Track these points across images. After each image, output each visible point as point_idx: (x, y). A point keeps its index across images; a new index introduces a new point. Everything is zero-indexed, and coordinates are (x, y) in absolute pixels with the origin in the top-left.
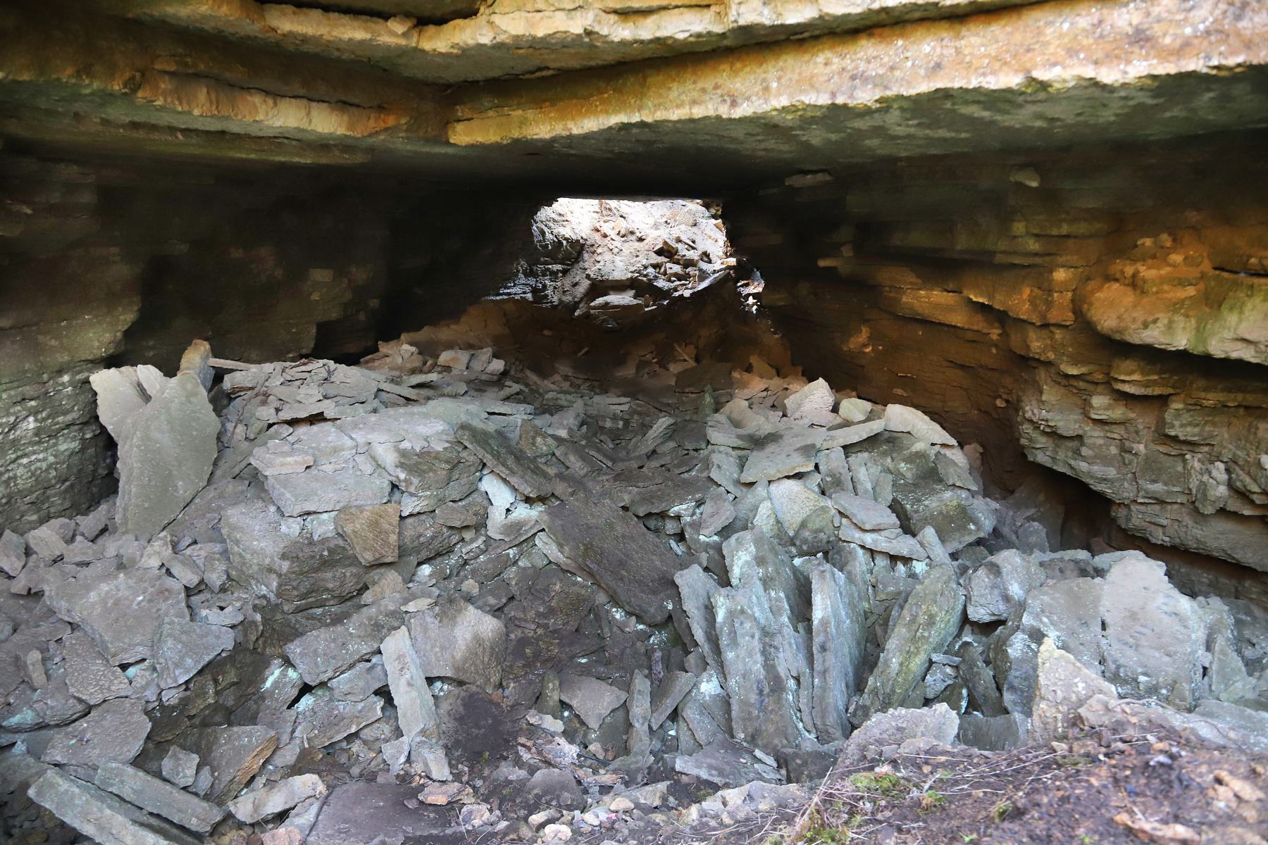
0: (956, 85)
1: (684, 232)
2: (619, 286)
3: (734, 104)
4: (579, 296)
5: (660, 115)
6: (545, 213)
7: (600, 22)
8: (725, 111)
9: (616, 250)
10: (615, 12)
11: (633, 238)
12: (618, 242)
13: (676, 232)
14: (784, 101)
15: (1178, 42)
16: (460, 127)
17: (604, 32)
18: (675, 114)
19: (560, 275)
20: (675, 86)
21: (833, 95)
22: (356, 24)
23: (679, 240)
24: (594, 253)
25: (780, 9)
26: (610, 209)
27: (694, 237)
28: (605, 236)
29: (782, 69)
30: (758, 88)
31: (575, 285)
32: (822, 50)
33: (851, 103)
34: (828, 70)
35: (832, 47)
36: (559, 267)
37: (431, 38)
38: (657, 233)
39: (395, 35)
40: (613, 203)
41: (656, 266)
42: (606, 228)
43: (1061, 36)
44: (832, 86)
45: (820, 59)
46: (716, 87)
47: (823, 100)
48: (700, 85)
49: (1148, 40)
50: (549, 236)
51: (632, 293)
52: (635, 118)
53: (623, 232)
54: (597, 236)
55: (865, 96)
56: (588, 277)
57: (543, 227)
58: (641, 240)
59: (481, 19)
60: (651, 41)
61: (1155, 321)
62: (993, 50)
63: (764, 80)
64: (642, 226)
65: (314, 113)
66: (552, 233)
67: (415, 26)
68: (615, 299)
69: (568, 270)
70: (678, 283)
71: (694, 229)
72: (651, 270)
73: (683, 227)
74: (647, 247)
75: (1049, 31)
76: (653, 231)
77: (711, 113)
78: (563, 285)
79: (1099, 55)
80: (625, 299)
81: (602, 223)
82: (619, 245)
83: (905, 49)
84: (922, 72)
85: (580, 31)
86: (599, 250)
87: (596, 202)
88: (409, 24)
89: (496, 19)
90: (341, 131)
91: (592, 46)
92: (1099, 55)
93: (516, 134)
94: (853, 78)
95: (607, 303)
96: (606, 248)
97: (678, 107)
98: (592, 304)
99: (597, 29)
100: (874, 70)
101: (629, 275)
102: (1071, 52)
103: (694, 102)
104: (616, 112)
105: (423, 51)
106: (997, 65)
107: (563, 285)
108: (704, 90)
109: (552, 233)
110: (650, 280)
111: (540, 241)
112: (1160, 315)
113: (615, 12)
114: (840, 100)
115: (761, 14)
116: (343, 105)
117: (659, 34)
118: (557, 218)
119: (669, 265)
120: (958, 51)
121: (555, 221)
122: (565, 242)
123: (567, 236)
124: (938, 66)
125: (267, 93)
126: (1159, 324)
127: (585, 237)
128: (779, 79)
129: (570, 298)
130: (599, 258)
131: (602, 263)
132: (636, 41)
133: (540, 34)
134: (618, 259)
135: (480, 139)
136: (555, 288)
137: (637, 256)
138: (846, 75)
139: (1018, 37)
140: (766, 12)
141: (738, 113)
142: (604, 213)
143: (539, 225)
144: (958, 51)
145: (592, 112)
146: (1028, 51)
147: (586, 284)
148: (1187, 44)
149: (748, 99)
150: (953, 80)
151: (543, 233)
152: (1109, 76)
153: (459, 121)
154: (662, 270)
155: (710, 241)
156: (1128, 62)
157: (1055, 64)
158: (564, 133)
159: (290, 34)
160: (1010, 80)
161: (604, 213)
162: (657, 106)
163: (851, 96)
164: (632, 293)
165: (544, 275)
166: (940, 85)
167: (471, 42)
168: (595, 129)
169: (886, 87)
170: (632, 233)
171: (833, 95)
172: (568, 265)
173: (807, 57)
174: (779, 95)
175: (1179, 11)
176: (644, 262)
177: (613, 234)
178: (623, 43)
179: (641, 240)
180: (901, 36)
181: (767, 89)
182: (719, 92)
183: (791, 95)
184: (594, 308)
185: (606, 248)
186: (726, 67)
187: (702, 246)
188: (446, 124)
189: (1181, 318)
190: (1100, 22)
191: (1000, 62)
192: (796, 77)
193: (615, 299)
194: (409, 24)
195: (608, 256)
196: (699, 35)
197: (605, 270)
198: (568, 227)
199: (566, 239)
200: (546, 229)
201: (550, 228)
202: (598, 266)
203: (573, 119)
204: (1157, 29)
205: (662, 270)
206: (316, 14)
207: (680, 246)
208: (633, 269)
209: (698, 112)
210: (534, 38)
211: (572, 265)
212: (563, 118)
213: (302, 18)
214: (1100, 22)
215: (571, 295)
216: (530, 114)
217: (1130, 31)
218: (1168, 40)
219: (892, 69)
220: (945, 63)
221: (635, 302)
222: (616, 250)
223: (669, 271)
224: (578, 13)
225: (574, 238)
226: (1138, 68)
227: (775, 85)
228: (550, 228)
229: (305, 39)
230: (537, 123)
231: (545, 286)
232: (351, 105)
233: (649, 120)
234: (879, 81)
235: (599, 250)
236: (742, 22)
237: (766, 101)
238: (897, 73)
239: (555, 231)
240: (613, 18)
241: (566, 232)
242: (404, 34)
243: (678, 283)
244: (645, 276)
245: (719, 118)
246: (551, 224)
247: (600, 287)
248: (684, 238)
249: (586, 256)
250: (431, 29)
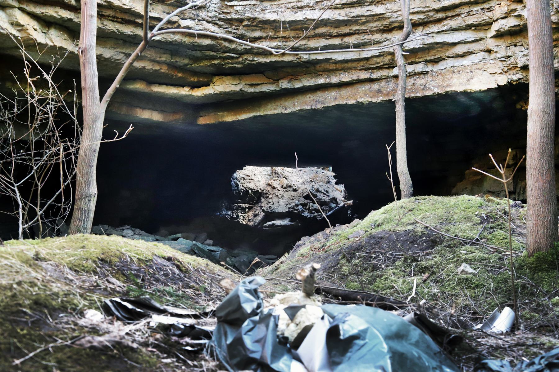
0: (341, 103)
1: (321, 186)
2: (281, 216)
3: (286, 109)
4: (258, 221)
5: (265, 113)
6: (239, 174)
7: (244, 88)
8: (283, 111)
9: (280, 196)
10: (249, 85)
11: (291, 189)
12: (282, 191)
13: (316, 186)
14: (299, 108)
15: (387, 92)
16: (201, 119)
17: (246, 90)
18: (269, 113)
19: (247, 210)
20: (269, 104)
21: (312, 106)
22: (175, 88)
23: (318, 190)
24: (267, 197)
25: (293, 84)
26: (278, 174)
27: (328, 189)
28: (274, 188)
29: (298, 99)
30: (292, 105)
31: (255, 216)
32: (308, 94)
33: (316, 108)
34: (310, 99)
35: (311, 93)
36: (247, 205)
37: (196, 92)
38: (304, 187)
39: (186, 91)
40: (279, 169)
41: (304, 205)
42: (275, 184)
43: (363, 91)
44: (311, 104)
45: (308, 97)
46: (281, 105)
47: (309, 108)
48: (276, 104)
49: (381, 92)
50: (241, 187)
51: (289, 219)
52: (258, 114)
53: (285, 186)
54: (269, 188)
55: (319, 106)
56: (263, 211)
57: (238, 182)
58: (295, 190)
59: (211, 87)
60: (259, 92)
61: (466, 188)
62: (348, 94)
63: (294, 102)
64: (296, 183)
65: (153, 114)
66: (243, 186)
67: (191, 89)
68: (278, 222)
69: (252, 207)
70: (316, 214)
71: (328, 185)
72: (300, 207)
73: (321, 184)
74: (299, 195)
75: (360, 89)
76: (303, 186)
77: (280, 112)
78: (249, 216)
79: (371, 95)
80: (285, 222)
81: (272, 181)
82: (282, 193)
83: (328, 94)
84: (332, 100)
85: (238, 90)
86: (270, 196)
87: (269, 169)
88: (189, 88)
89: (214, 87)
90: (161, 120)
91: (242, 94)
92: (371, 95)
93: (220, 120)
94: (316, 101)
95: (273, 224)
96: (274, 195)
97: (270, 110)
98: (265, 225)
99: (243, 89)
100: (321, 99)
101: (287, 210)
102: (365, 95)
103: (275, 109)
104: (252, 112)
105: (193, 95)
106: (350, 98)
107: (249, 216)
108: (277, 105)
109: (243, 186)
110: (299, 212)
111: (235, 190)
112: (468, 186)
113: (249, 85)
114: (313, 108)
115: (287, 85)
116: (162, 111)
117: (261, 90)
118: (246, 177)
119: (311, 204)
120: (340, 95)
121: (244, 179)
122: (250, 191)
123: (252, 188)
124: (336, 98)
125: (141, 108)
126: (467, 189)
127: (262, 189)
128: (298, 102)
129: (253, 223)
130: (270, 201)
131: (272, 203)
132: (255, 92)
133: (227, 91)
134: (281, 201)
135: (208, 122)
136: (244, 217)
137: (293, 199)
138: (314, 101)
139: (353, 91)
140: (289, 85)
141: (287, 112)
142: (274, 175)
143: (235, 181)
144: (340, 95)
145: (245, 112)
146: (356, 94)
147: (262, 215)
148: (389, 93)
149: (290, 108)
150: (340, 102)
151: (237, 185)
152: (374, 100)
153: (201, 116)
154: (308, 207)
155: (337, 192)
156: (378, 97)
157: (362, 98)
158: (236, 119)
159: (157, 92)
160: (353, 102)
161: (274, 175)
162: (264, 110)
163: (316, 107)
164: (289, 219)
165: (237, 210)
166: (337, 103)
167: (208, 93)
168: (246, 118)
169: (324, 104)
170: (290, 187)
171: (312, 106)
172: (252, 204)
173: (305, 96)
174: (297, 107)
175: (386, 85)
176: (297, 202)
177: (279, 187)
178: (251, 93)
179: (295, 190)
180: (327, 90)
181: (294, 105)
182: (282, 106)
183: (301, 107)
184: (266, 227)
185: (274, 195)
186: (283, 99)
187: (332, 194)
188: (196, 118)
189: (476, 187)
190: (370, 87)
191: (350, 97)
192: (302, 101)
193: (278, 222)
194: (189, 88)
195: (275, 199)
196: (273, 90)
197: (273, 207)
198: (252, 183)
199: (251, 189)
200: (239, 184)
201: (241, 183)
202: (269, 205)
203: (239, 115)
204: (382, 89)
205: (308, 207)
206: (164, 86)
207: (318, 194)
208: (290, 206)
209: (276, 112)
210: (226, 92)
211: (254, 204)
212: (236, 115)
213: (160, 87)
214: (370, 87)
215: (253, 221)
216: (225, 113)
217: (377, 89)
218: (385, 92)
219: (325, 99)
220: (337, 98)
221: (290, 223)
222: (280, 196)
223: (311, 208)
224: (238, 85)
225: (256, 189)
226: (380, 99)
227: (296, 104)
228: (241, 183)
229: (160, 92)
230: (227, 116)
231: (238, 216)
232: (164, 112)
233: (262, 114)
234: (322, 103)
235: (270, 196)
236: (283, 87)
237: (294, 108)
238: (327, 100)
239: (245, 185)
240: (248, 86)
241: (251, 185)
242: (188, 91)
243: (316, 214)
244: (297, 210)
245: (282, 113)
246: (242, 181)
247: (270, 216)
248: (321, 189)
249: (262, 199)
250: (196, 89)
